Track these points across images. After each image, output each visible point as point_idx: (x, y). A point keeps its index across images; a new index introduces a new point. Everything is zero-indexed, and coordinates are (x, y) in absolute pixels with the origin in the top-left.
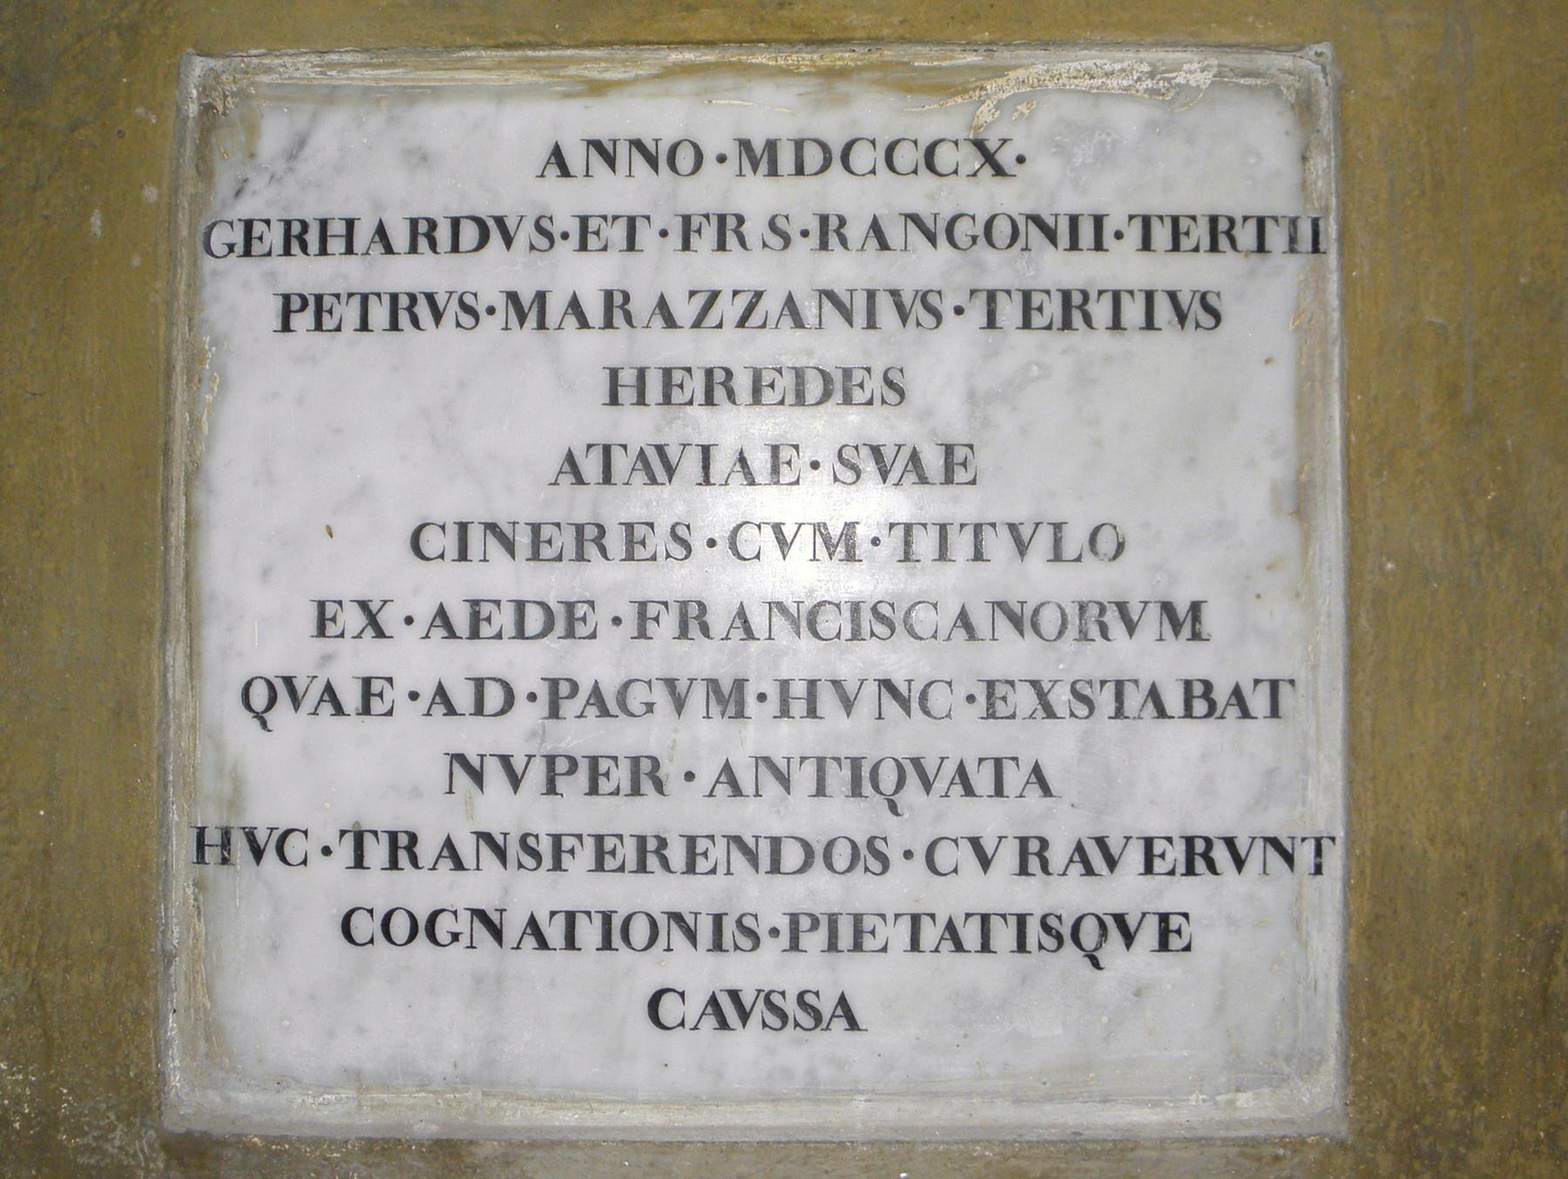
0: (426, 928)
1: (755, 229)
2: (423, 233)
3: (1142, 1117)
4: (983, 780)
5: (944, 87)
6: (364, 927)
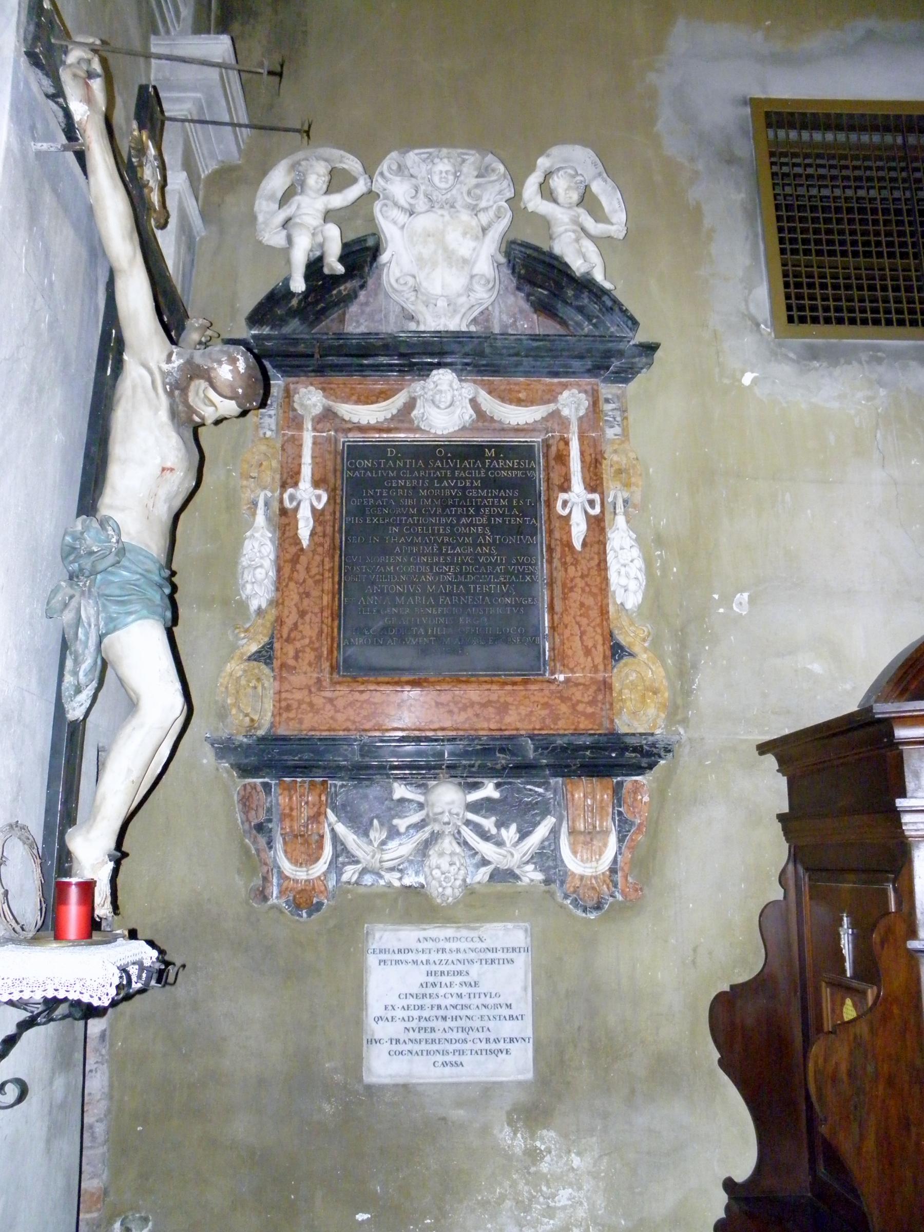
0: (401, 1053)
1: (447, 950)
2: (400, 951)
3: (504, 1079)
4: (480, 1030)
5: (474, 929)
6: (392, 1053)
